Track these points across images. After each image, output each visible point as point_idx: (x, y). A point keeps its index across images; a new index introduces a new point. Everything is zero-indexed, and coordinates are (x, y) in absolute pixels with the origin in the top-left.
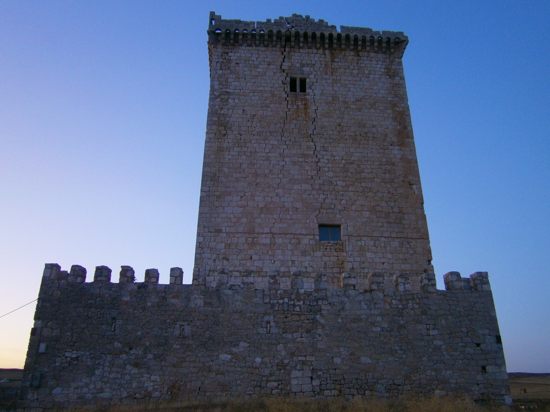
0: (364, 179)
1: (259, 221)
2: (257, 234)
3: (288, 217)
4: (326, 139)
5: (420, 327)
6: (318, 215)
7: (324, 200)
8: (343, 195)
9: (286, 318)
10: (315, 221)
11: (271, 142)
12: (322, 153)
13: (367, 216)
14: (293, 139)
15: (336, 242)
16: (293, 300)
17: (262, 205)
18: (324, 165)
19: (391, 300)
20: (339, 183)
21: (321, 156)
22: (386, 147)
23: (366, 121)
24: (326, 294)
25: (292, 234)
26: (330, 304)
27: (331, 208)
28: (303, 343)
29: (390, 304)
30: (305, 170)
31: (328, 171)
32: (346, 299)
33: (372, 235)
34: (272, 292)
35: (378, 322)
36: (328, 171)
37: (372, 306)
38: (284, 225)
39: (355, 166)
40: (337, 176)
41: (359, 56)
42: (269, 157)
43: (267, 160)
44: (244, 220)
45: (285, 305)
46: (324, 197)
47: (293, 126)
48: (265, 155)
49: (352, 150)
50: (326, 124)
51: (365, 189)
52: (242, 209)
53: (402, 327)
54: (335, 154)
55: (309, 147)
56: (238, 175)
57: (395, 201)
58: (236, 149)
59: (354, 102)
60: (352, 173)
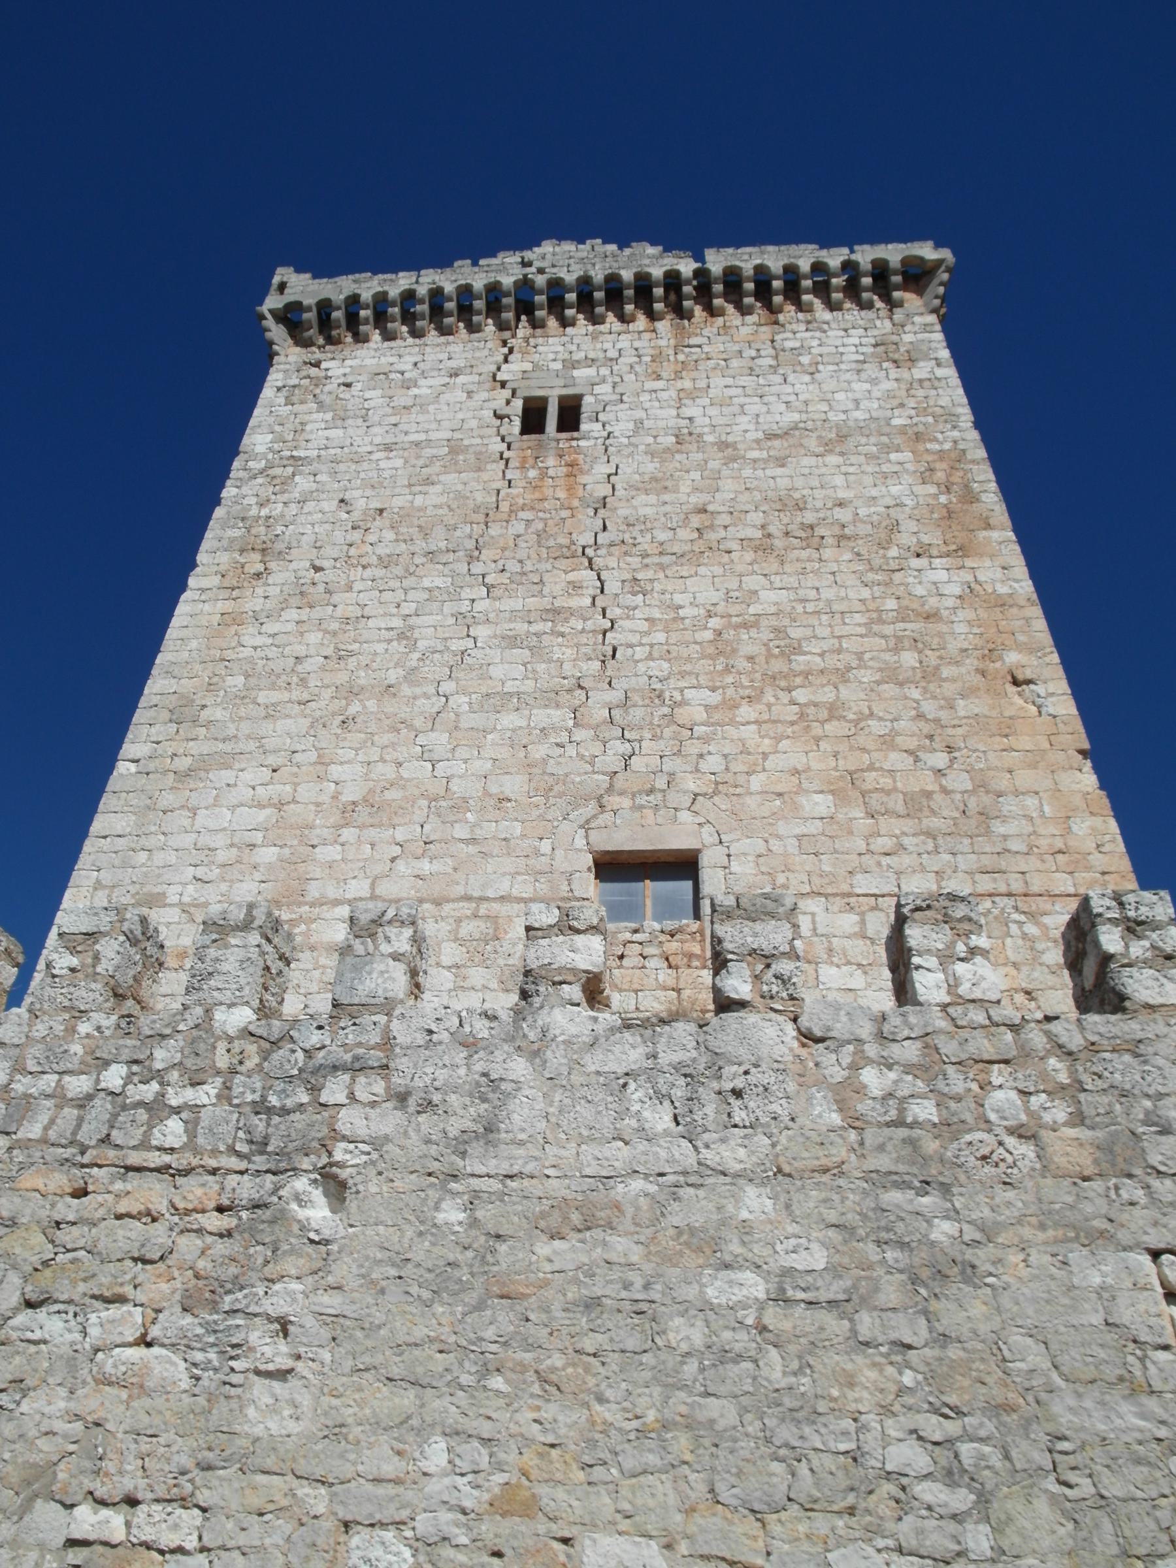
0: (806, 674)
1: (331, 853)
2: (312, 905)
3: (461, 832)
4: (645, 555)
5: (1094, 1271)
6: (595, 817)
7: (627, 759)
8: (706, 740)
9: (81, 1193)
10: (580, 842)
11: (426, 583)
12: (629, 600)
13: (823, 811)
14: (513, 566)
15: (670, 925)
16: (158, 1075)
17: (350, 794)
18: (634, 639)
19: (855, 1067)
20: (690, 694)
21: (618, 611)
22: (893, 565)
23: (805, 492)
24: (387, 1030)
25: (467, 898)
26: (402, 1098)
27: (651, 791)
28: (134, 1385)
29: (846, 1094)
30: (550, 661)
31: (650, 657)
32: (519, 1068)
33: (845, 888)
34: (40, 1030)
35: (746, 1228)
36: (650, 657)
37: (710, 1109)
38: (436, 867)
39: (766, 635)
40: (683, 675)
41: (776, 323)
42: (411, 628)
43: (402, 636)
44: (268, 855)
45: (101, 1108)
46: (626, 748)
47: (518, 527)
48: (397, 622)
49: (751, 582)
50: (649, 511)
51: (811, 710)
52: (268, 811)
53: (939, 1273)
54: (678, 599)
55: (576, 586)
56: (276, 696)
57: (950, 749)
58: (292, 614)
59: (758, 441)
60: (751, 659)
